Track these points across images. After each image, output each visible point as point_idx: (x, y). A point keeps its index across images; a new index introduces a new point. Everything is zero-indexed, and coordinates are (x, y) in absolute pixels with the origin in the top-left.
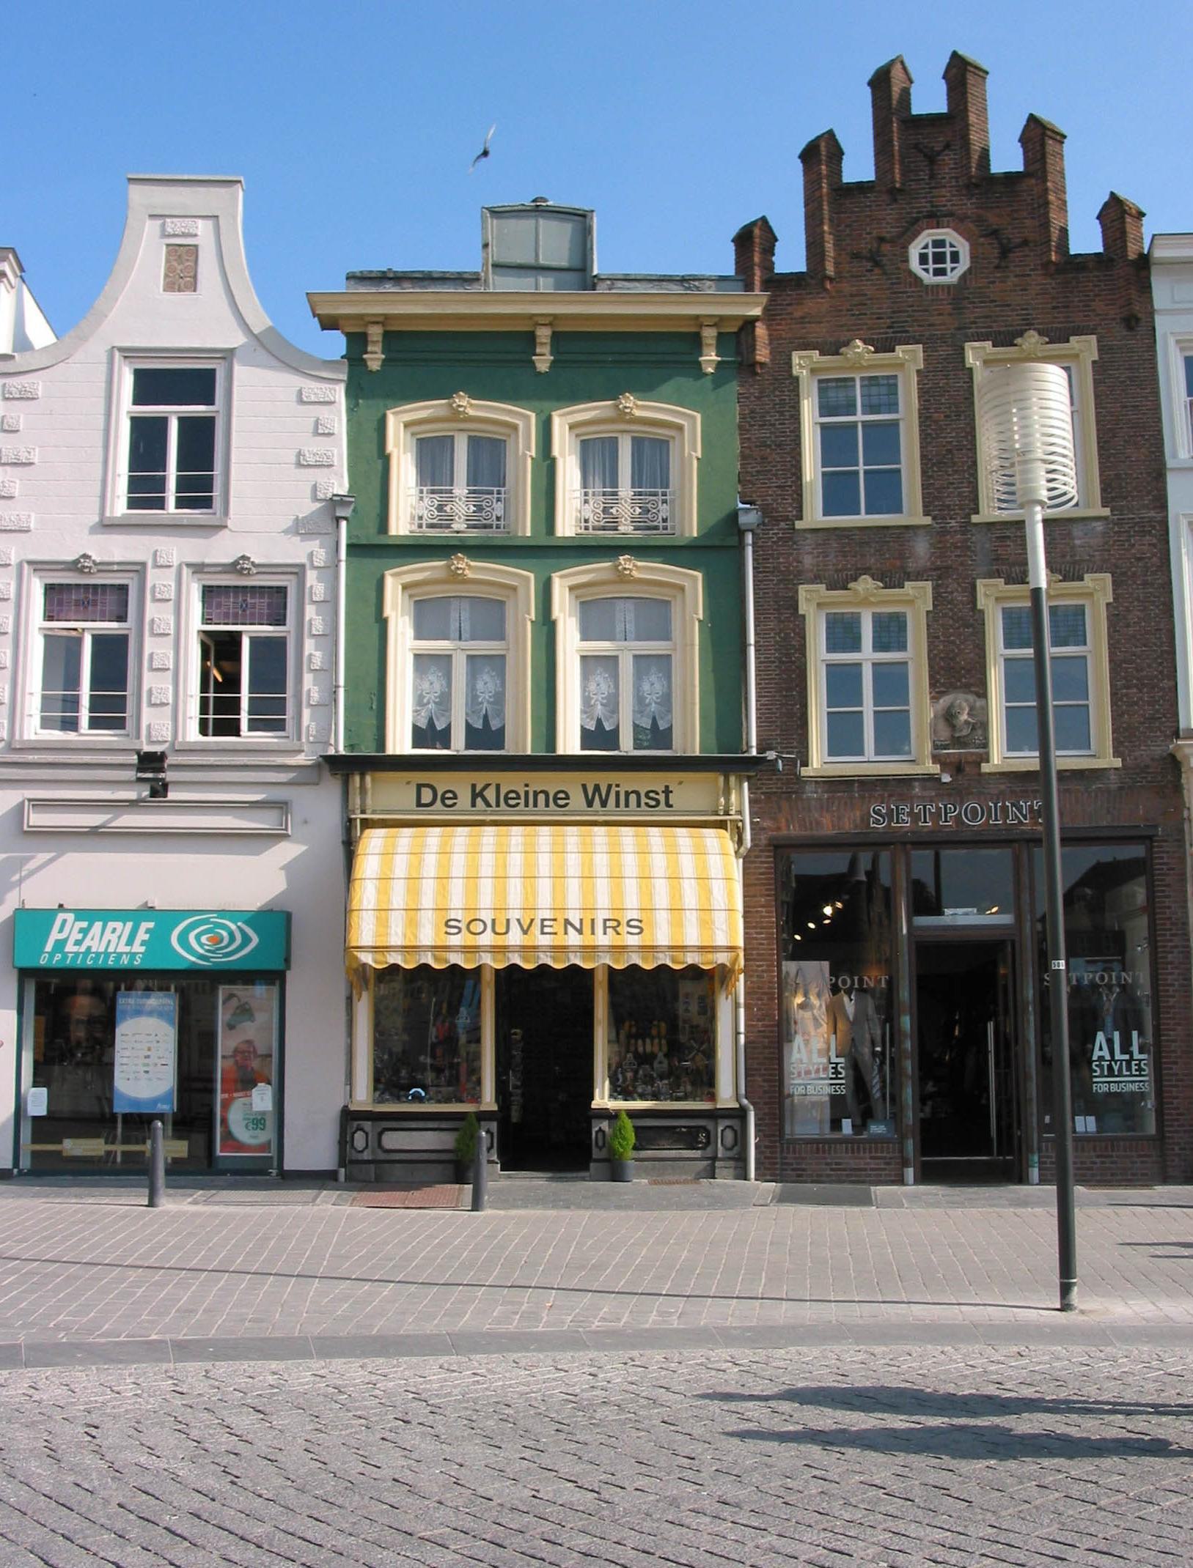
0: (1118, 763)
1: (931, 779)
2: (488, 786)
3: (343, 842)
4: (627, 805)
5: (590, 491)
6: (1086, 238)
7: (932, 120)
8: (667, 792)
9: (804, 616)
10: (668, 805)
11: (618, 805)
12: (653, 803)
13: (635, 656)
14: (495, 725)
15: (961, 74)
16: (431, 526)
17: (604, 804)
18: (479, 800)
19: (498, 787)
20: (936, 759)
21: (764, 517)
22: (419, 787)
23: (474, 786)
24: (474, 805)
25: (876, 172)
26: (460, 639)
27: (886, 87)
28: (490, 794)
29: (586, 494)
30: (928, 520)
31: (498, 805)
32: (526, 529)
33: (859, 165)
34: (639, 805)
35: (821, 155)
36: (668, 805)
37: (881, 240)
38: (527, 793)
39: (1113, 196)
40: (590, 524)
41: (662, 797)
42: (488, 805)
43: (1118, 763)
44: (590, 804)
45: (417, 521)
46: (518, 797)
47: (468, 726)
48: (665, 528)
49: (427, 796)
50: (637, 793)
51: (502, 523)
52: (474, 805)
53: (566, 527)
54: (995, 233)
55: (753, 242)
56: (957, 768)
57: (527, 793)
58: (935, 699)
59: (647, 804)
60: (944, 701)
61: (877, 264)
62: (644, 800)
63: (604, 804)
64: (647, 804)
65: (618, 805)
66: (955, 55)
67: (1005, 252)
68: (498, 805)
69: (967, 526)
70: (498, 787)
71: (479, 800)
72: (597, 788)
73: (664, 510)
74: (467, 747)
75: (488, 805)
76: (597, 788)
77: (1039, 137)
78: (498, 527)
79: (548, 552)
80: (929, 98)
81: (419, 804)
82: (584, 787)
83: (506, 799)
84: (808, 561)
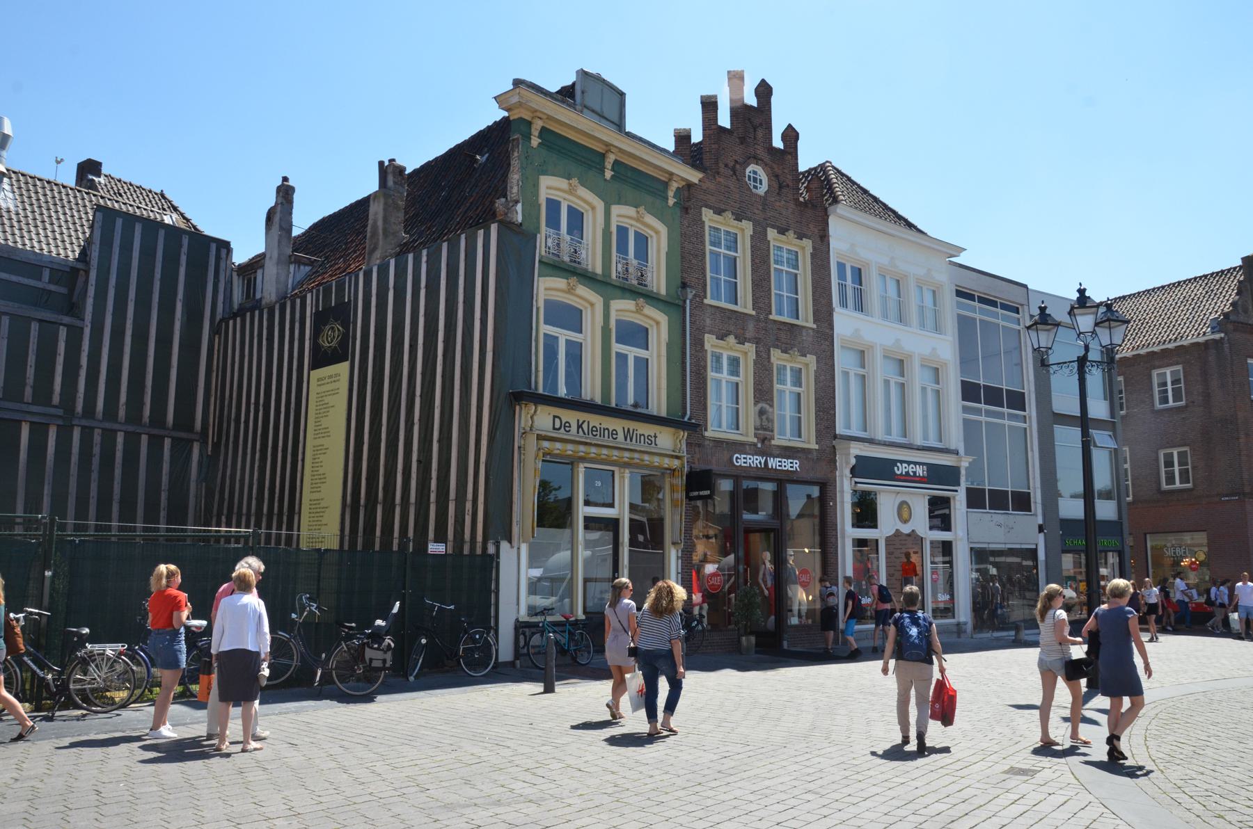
0: (817, 447)
1: (755, 445)
6: (778, 143)
9: (1243, 259)
15: (764, 91)
20: (756, 435)
21: (1192, 356)
22: (555, 417)
25: (1057, 505)
26: (901, 319)
28: (585, 426)
30: (754, 313)
37: (736, 162)
39: (763, 81)
43: (817, 447)
54: (777, 176)
56: (763, 440)
58: (756, 403)
60: (760, 405)
61: (735, 173)
66: (763, 81)
67: (781, 187)
69: (767, 318)
77: (791, 135)
84: (708, 321)
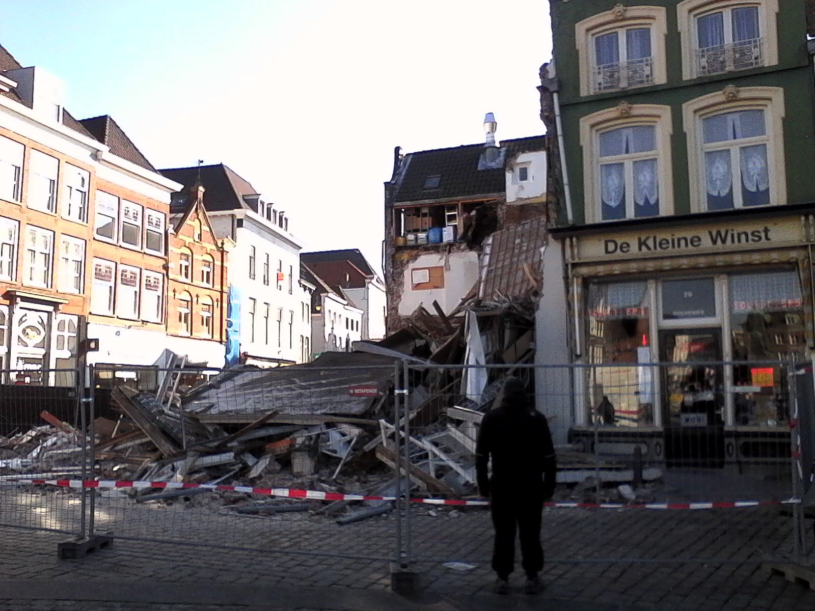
2: (647, 238)
3: (564, 278)
4: (739, 241)
5: (601, 66)
8: (766, 231)
10: (767, 238)
11: (733, 241)
12: (756, 239)
13: (635, 162)
14: (762, 188)
16: (605, 88)
17: (724, 241)
18: (644, 248)
19: (655, 238)
23: (640, 239)
24: (640, 249)
28: (650, 243)
29: (599, 69)
31: (655, 247)
32: (660, 77)
34: (747, 240)
36: (767, 238)
38: (673, 240)
40: (602, 86)
41: (763, 235)
42: (649, 248)
44: (714, 242)
45: (597, 86)
46: (668, 242)
47: (636, 204)
48: (756, 63)
49: (611, 247)
50: (686, 239)
51: (650, 78)
52: (640, 249)
53: (689, 72)
57: (673, 240)
59: (753, 240)
62: (750, 237)
63: (724, 241)
64: (753, 240)
65: (733, 241)
68: (655, 247)
70: (655, 238)
71: (644, 248)
72: (719, 233)
73: (647, 70)
74: (604, 218)
75: (649, 248)
76: (719, 233)
78: (647, 81)
79: (675, 92)
81: (607, 252)
82: (710, 233)
83: (660, 244)
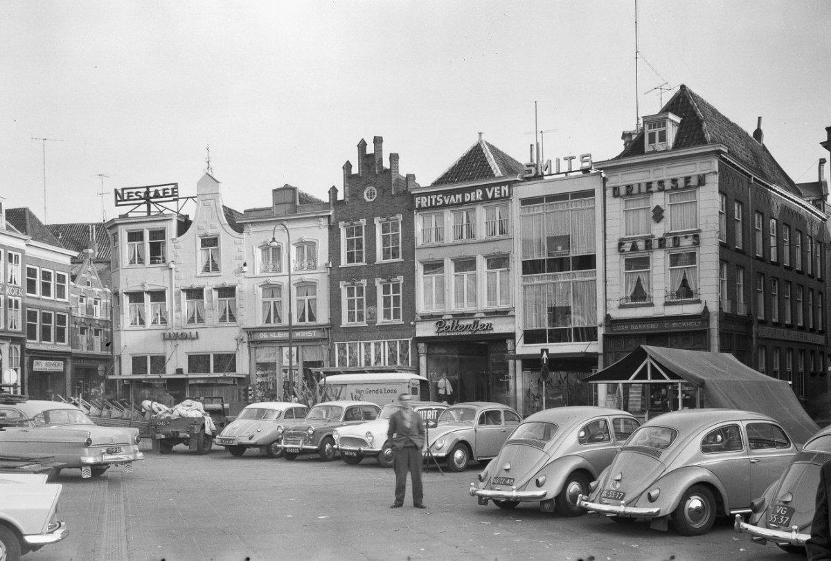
7: (370, 155)
27: (362, 146)
33: (355, 170)
35: (348, 166)
55: (333, 191)
77: (394, 158)
80: (370, 149)
